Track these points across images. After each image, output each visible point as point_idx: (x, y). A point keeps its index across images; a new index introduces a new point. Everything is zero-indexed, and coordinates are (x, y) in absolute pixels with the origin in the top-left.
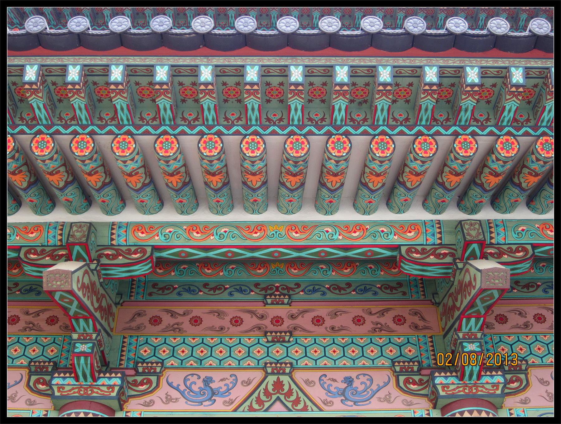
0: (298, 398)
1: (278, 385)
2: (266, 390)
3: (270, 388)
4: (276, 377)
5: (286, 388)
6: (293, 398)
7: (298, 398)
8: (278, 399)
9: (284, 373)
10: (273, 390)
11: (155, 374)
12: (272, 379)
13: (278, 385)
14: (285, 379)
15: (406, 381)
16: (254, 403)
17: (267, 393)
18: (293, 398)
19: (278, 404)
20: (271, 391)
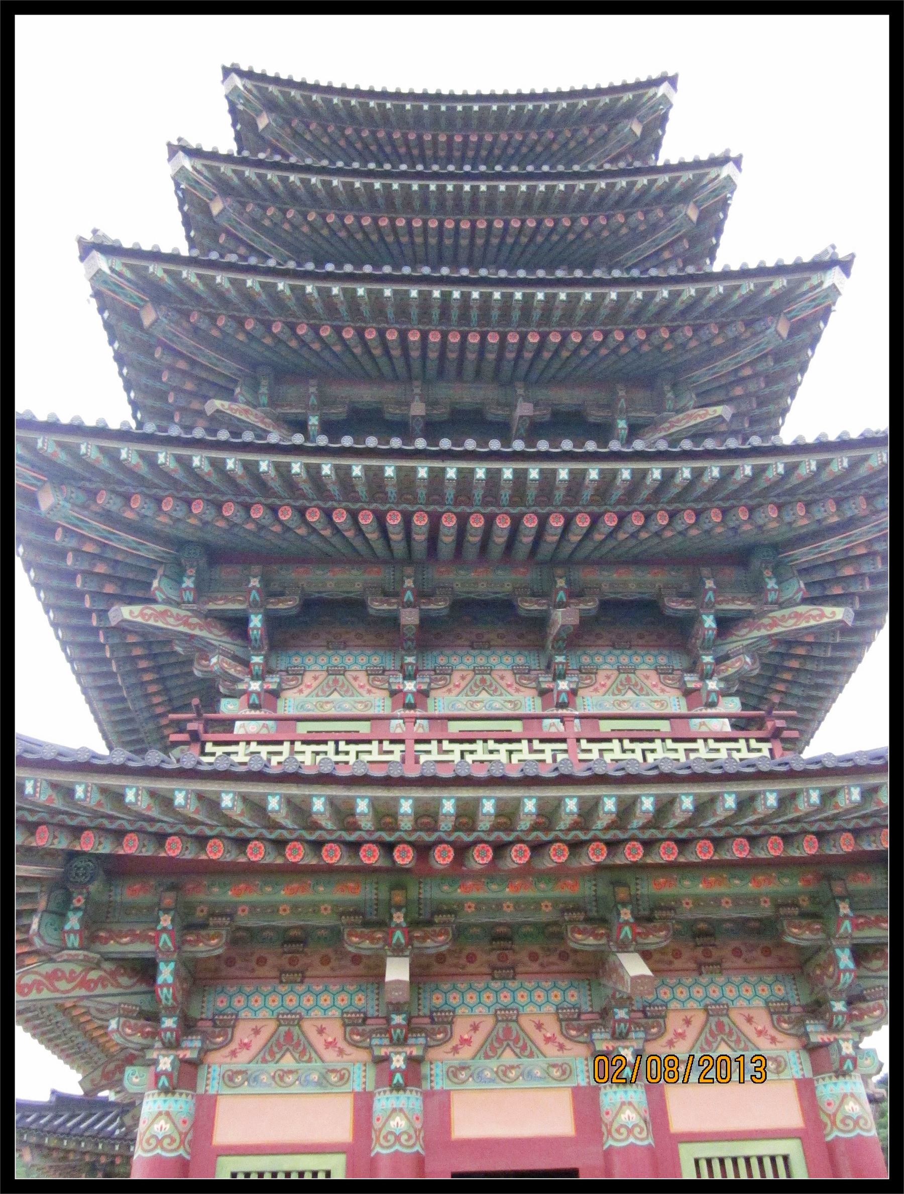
0: (738, 1037)
2: (278, 1041)
6: (521, 1044)
12: (283, 1029)
14: (725, 1020)
15: (779, 1021)
18: (521, 1044)
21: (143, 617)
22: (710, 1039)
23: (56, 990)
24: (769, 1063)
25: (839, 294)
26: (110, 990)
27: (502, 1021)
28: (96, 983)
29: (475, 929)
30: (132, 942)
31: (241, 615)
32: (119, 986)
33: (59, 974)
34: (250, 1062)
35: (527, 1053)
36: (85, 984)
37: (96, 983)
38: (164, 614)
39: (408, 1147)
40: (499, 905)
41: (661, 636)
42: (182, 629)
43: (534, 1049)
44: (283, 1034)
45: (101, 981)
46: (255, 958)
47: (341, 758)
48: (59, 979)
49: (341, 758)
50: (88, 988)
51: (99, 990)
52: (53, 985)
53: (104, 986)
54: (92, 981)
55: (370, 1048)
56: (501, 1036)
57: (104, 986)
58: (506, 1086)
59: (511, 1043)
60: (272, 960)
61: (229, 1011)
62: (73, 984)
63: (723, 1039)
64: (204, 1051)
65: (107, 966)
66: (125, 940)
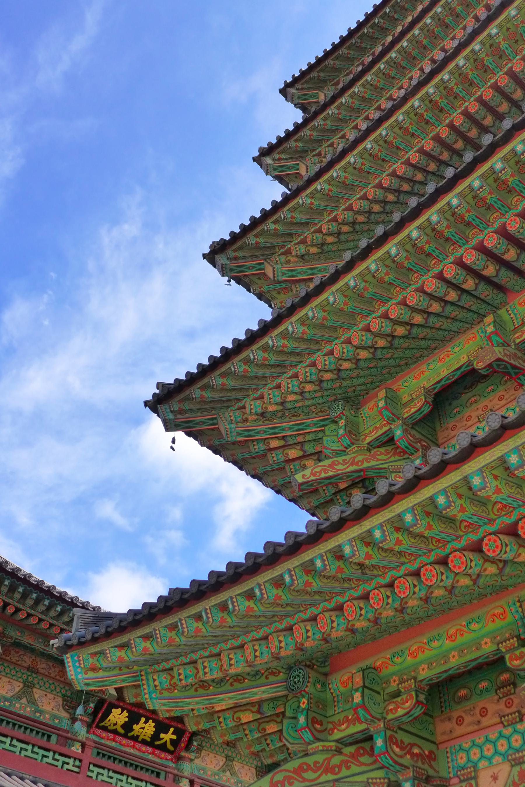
21: (315, 475)
23: (305, 780)
24: (312, 738)
25: (170, 589)
26: (355, 769)
28: (340, 767)
30: (348, 727)
32: (362, 764)
33: (305, 767)
36: (329, 770)
37: (340, 767)
38: (331, 466)
40: (445, 657)
42: (351, 468)
44: (516, 773)
45: (345, 764)
46: (477, 711)
47: (12, 748)
48: (306, 771)
49: (12, 748)
50: (333, 773)
51: (344, 772)
52: (301, 777)
53: (348, 768)
54: (335, 766)
57: (348, 768)
60: (492, 708)
61: (470, 764)
62: (319, 773)
65: (350, 750)
66: (343, 727)
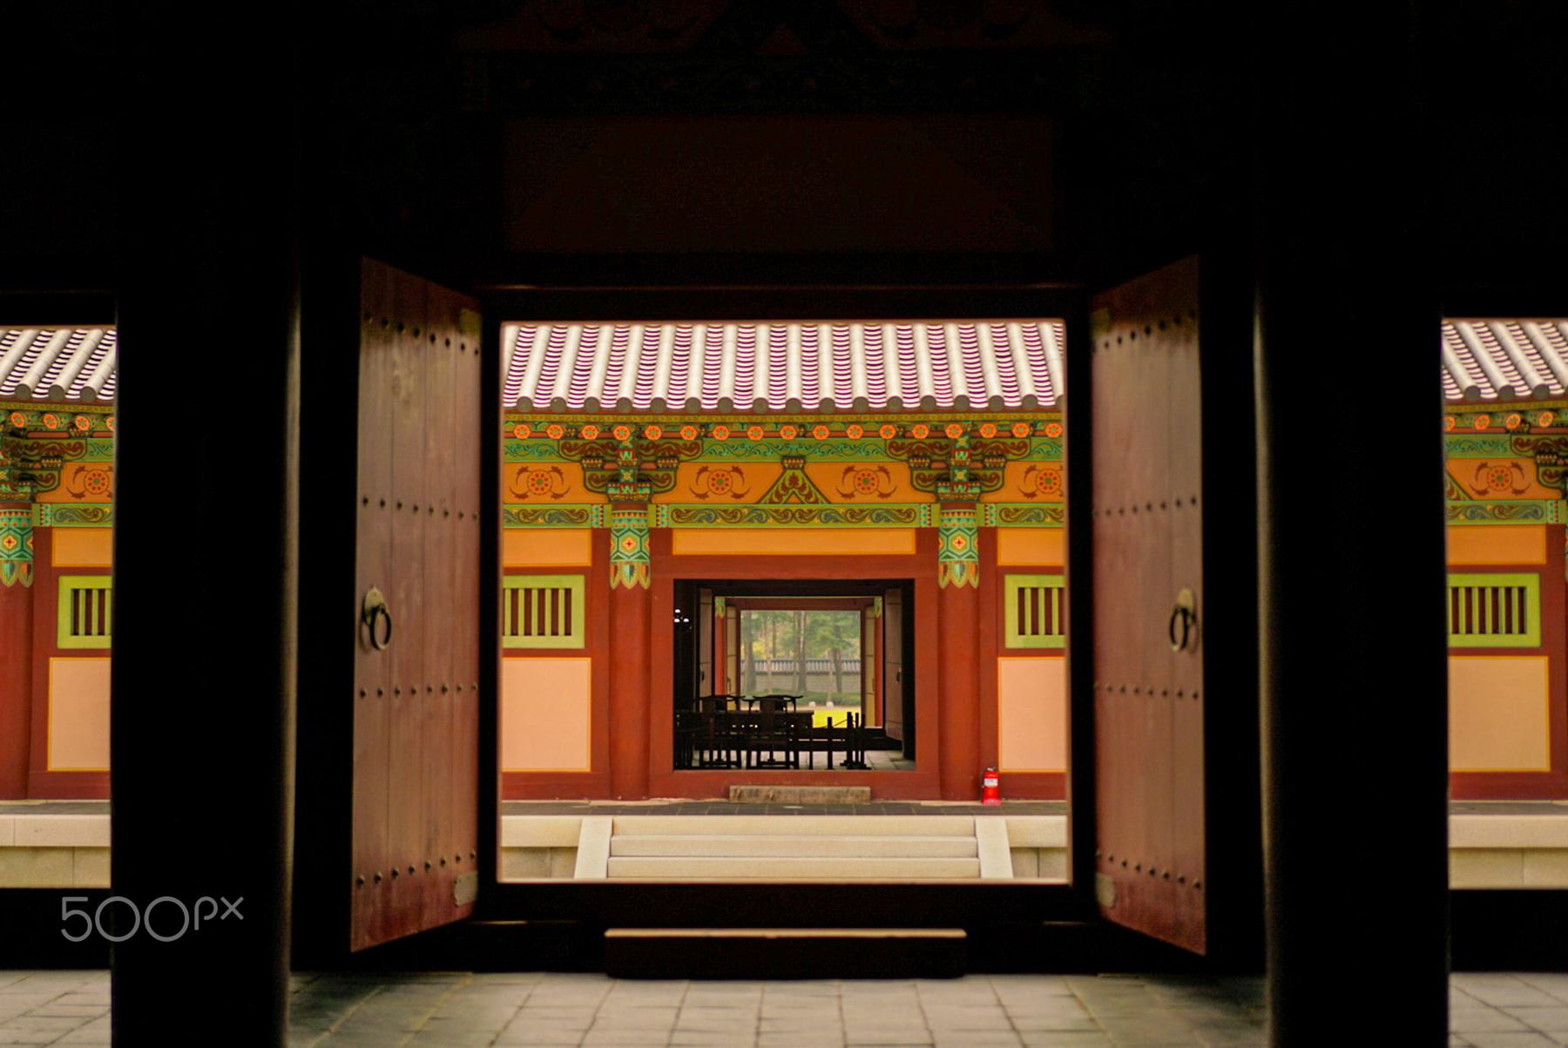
0: (810, 492)
1: (794, 480)
2: (783, 484)
3: (787, 483)
4: (792, 471)
5: (800, 483)
6: (806, 492)
7: (810, 492)
8: (794, 492)
9: (798, 468)
10: (790, 484)
11: (999, 468)
12: (789, 473)
13: (794, 480)
14: (798, 473)
16: (774, 496)
17: (784, 487)
18: (806, 492)
19: (794, 496)
20: (787, 485)
22: (782, 492)
27: (789, 468)
29: (1487, 450)
31: (1500, 630)
34: (758, 503)
35: (812, 500)
39: (966, 540)
41: (1276, 805)
43: (819, 496)
44: (788, 478)
55: (605, 493)
56: (787, 483)
58: (800, 526)
59: (797, 491)
63: (794, 492)
64: (653, 493)
